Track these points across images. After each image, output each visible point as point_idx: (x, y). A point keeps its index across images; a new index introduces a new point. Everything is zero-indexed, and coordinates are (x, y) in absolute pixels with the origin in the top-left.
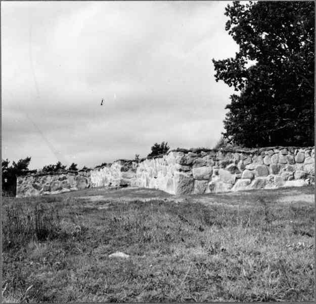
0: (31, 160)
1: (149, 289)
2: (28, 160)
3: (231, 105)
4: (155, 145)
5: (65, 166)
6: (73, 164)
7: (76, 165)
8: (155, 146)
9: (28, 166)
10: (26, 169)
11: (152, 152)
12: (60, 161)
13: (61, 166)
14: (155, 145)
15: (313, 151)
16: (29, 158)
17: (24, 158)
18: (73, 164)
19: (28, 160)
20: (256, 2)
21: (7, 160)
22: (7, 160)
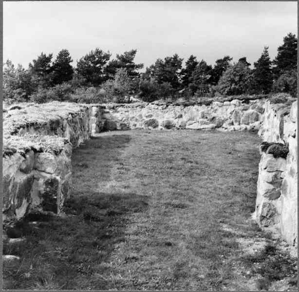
0: (137, 53)
1: (177, 207)
2: (134, 53)
3: (284, 45)
4: (289, 35)
5: (182, 58)
6: (192, 56)
7: (195, 58)
8: (288, 37)
9: (134, 59)
10: (131, 63)
11: (283, 44)
12: (177, 54)
13: (178, 59)
14: (289, 35)
15: (294, 109)
16: (134, 50)
17: (129, 50)
18: (192, 56)
19: (134, 53)
20: (3, 236)
21: (109, 52)
22: (109, 52)
